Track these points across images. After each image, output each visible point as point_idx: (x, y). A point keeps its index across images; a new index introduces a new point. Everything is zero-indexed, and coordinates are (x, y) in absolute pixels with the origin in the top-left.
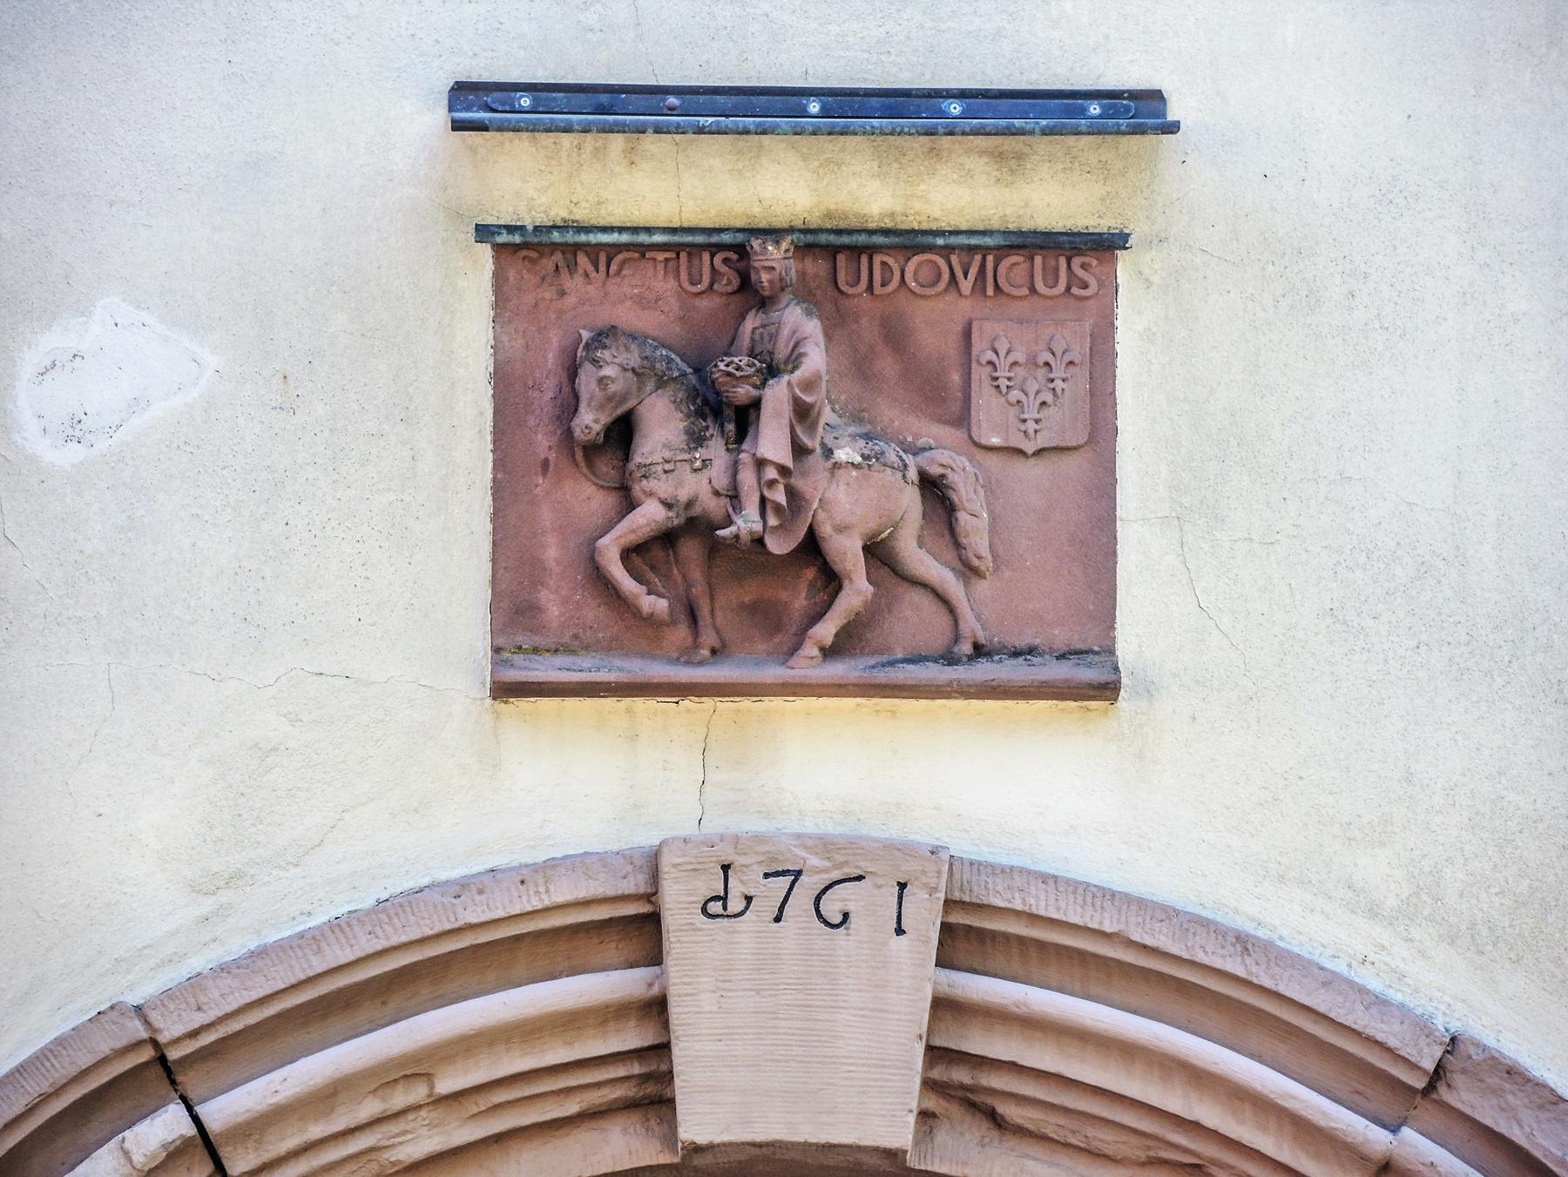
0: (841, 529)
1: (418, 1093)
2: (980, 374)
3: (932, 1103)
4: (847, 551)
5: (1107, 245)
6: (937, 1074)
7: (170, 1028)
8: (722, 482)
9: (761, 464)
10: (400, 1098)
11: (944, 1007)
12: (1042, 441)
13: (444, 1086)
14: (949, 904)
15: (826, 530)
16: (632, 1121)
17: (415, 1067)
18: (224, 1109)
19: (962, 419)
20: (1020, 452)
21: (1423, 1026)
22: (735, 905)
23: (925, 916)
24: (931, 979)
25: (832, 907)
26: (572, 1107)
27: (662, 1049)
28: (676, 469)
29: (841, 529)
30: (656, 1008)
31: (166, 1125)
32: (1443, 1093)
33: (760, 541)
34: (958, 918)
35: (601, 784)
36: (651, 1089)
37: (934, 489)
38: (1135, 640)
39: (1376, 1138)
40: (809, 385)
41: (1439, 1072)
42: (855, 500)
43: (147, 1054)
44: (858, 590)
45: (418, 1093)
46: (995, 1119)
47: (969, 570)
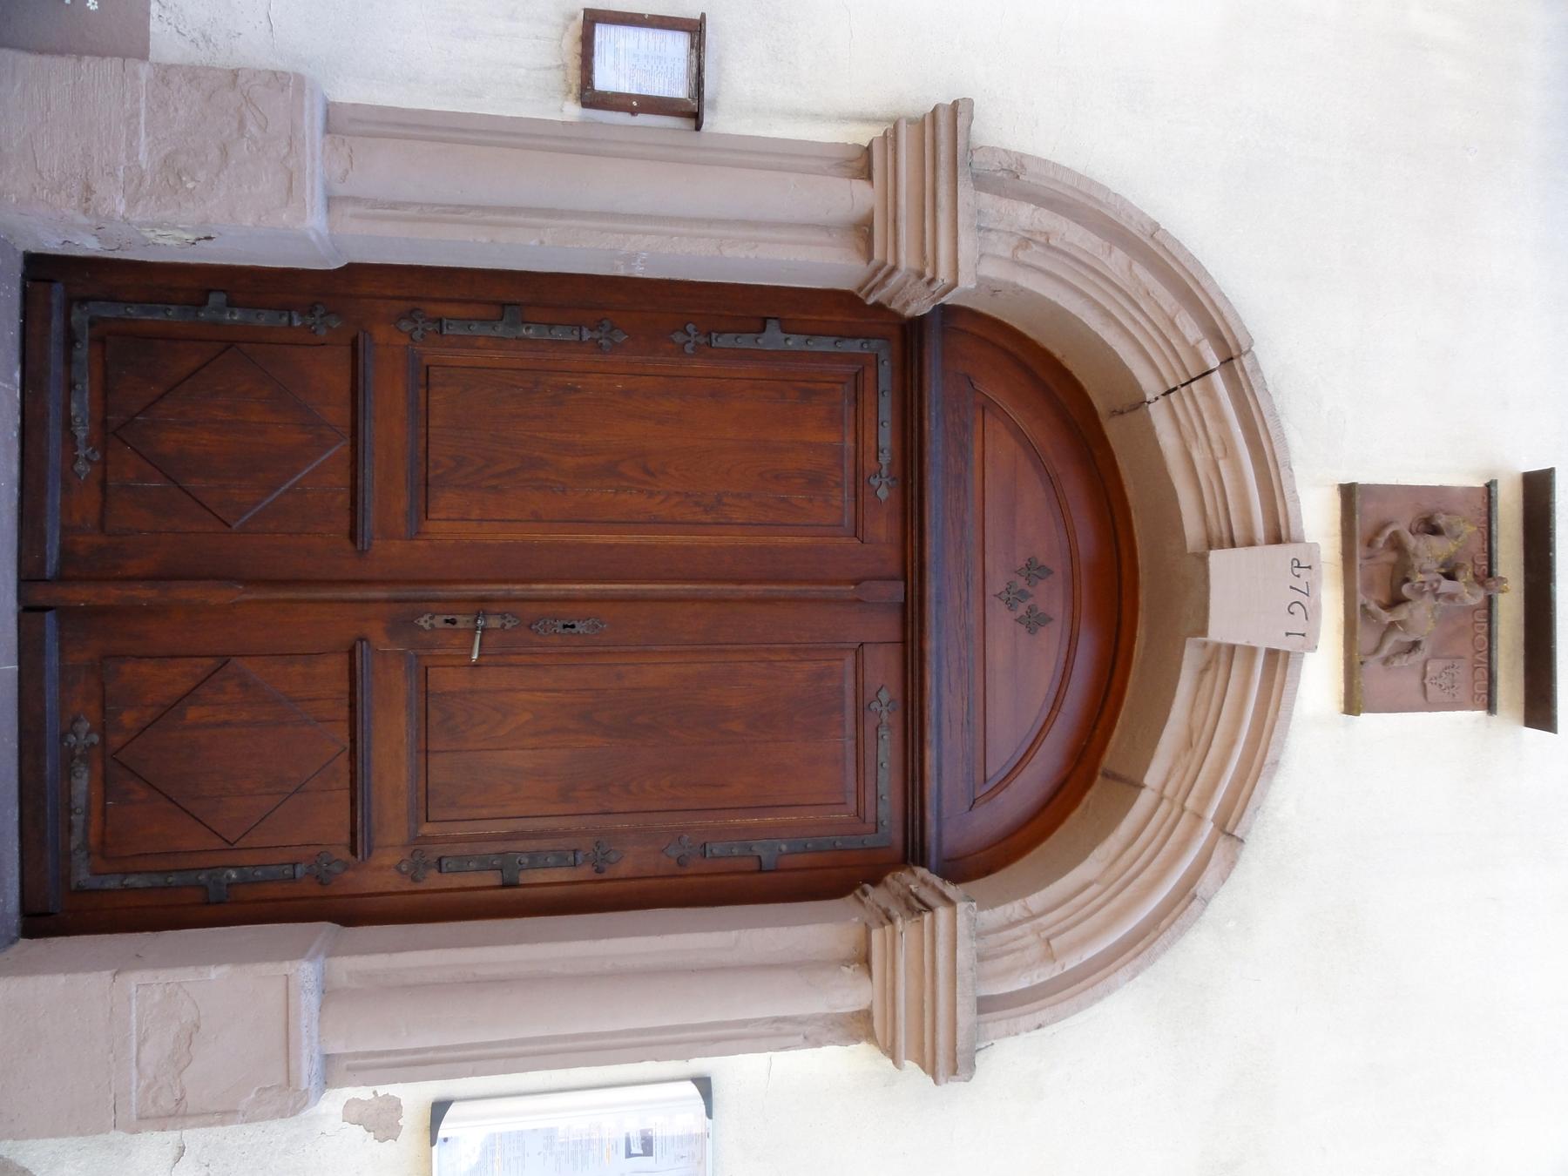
0: (1410, 611)
1: (1219, 453)
2: (1449, 663)
3: (1210, 648)
4: (1402, 613)
5: (1491, 707)
6: (1223, 649)
7: (1246, 361)
8: (1426, 567)
9: (1438, 581)
10: (1216, 446)
11: (1252, 651)
12: (1429, 686)
13: (1221, 463)
14: (1288, 653)
15: (1410, 605)
16: (1202, 535)
17: (1229, 449)
18: (1217, 378)
19: (1435, 657)
20: (1424, 677)
21: (1248, 832)
22: (1297, 571)
23: (1282, 645)
24: (1262, 645)
25: (1296, 607)
26: (1210, 511)
27: (1233, 545)
28: (1429, 552)
29: (1410, 611)
30: (1251, 543)
31: (1213, 361)
32: (1223, 837)
33: (1407, 580)
34: (1281, 657)
35: (1317, 519)
36: (1215, 541)
37: (1415, 645)
38: (1368, 721)
39: (1210, 814)
40: (1462, 599)
41: (1230, 835)
42: (1421, 616)
43: (1235, 353)
44: (1387, 617)
45: (1219, 453)
46: (1204, 671)
47: (1386, 661)
